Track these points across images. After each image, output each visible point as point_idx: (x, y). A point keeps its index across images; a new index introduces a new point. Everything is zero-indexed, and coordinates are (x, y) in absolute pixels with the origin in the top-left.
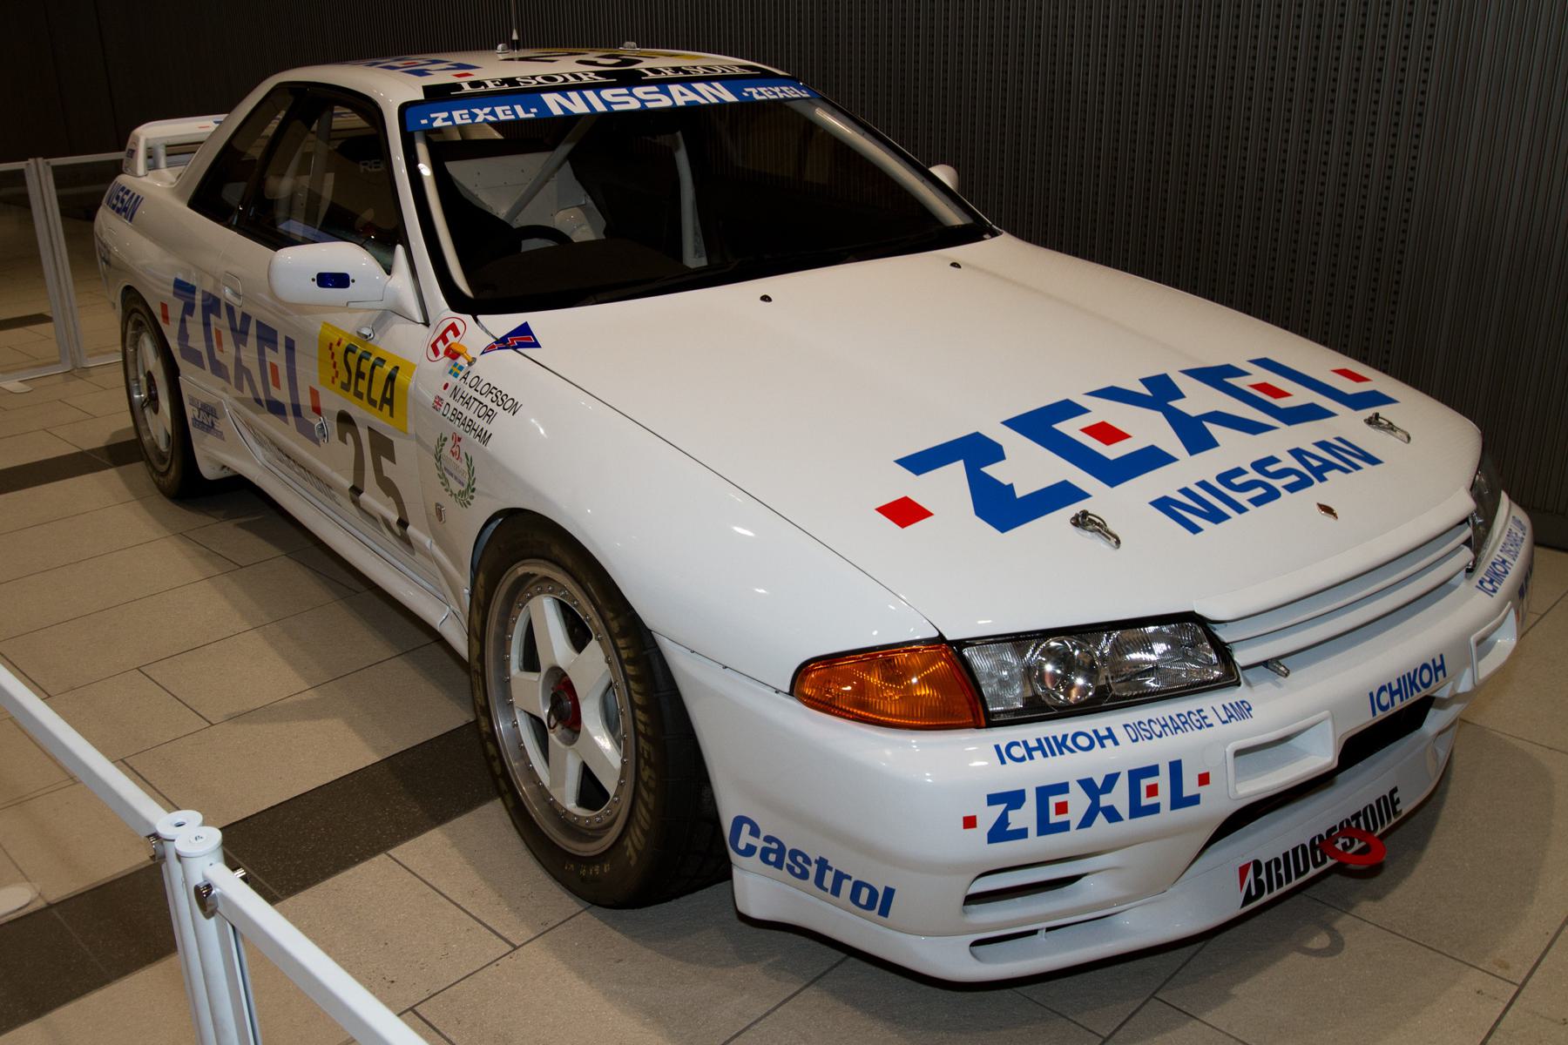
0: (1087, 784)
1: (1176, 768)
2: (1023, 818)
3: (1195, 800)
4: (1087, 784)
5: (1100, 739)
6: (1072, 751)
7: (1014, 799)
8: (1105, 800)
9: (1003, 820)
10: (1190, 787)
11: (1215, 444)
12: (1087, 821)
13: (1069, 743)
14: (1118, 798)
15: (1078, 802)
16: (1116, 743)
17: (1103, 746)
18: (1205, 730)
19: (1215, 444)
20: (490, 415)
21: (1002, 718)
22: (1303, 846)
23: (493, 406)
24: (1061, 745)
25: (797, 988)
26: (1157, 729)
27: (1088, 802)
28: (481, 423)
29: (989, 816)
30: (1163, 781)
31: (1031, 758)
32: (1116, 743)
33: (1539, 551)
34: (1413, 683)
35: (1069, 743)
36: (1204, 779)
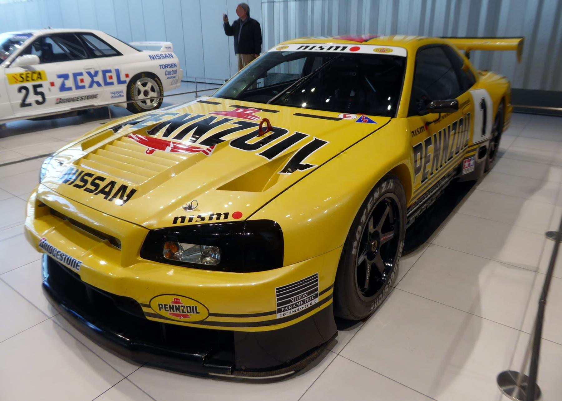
0: (89, 73)
1: (118, 72)
4: (89, 73)
8: (96, 79)
9: (63, 85)
12: (91, 86)
15: (87, 80)
30: (114, 75)
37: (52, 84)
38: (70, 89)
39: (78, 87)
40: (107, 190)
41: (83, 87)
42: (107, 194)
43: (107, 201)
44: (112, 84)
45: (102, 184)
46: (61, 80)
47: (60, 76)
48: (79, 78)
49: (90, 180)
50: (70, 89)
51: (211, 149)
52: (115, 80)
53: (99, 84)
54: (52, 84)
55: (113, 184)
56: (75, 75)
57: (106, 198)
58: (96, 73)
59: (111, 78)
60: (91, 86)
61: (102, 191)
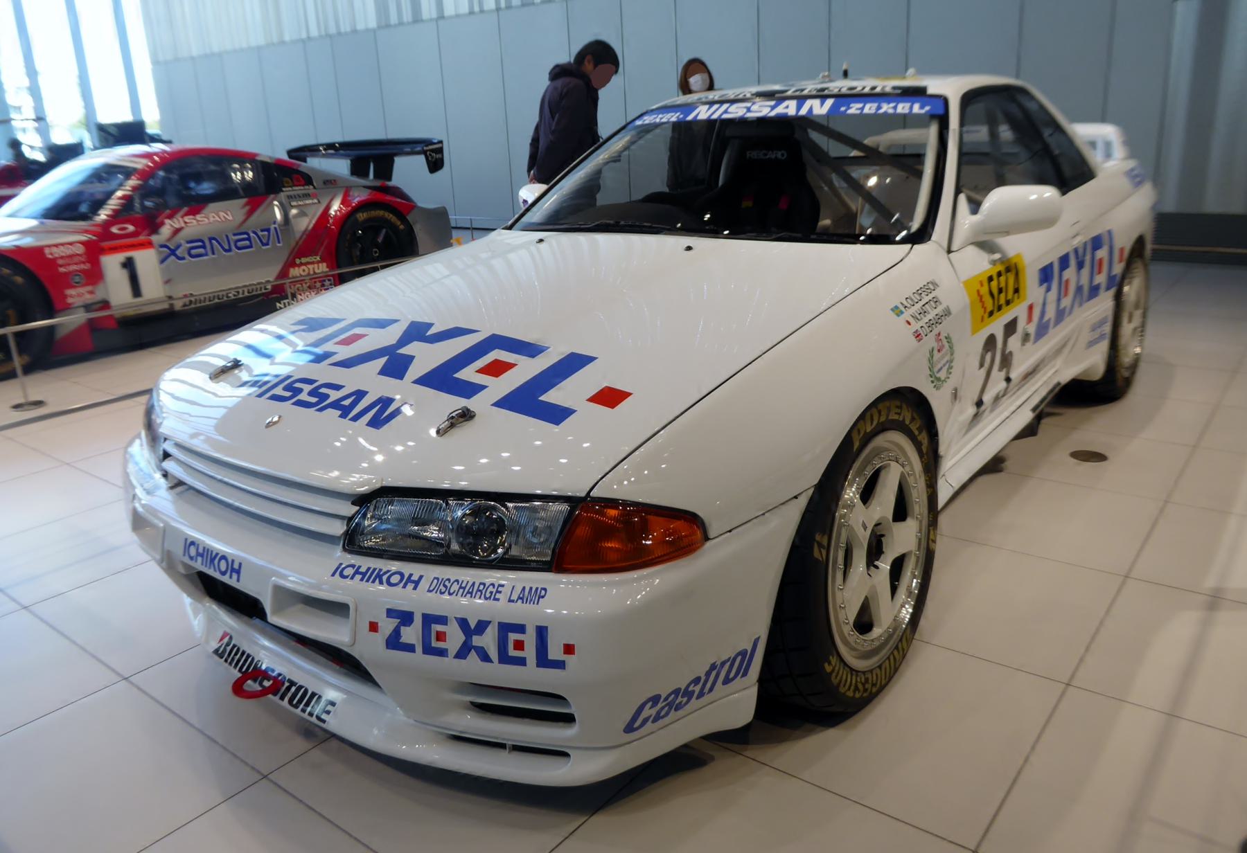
0: (463, 623)
1: (542, 632)
2: (411, 634)
3: (560, 665)
4: (463, 623)
5: (408, 581)
6: (381, 583)
7: (405, 618)
8: (477, 641)
9: (396, 633)
10: (555, 653)
11: (412, 358)
12: (462, 654)
13: (385, 578)
14: (488, 640)
15: (455, 639)
16: (415, 588)
17: (404, 587)
18: (491, 602)
19: (412, 358)
20: (936, 301)
21: (533, 565)
22: (306, 691)
23: (930, 296)
24: (379, 577)
25: (194, 721)
26: (455, 587)
27: (463, 638)
28: (939, 310)
29: (387, 626)
30: (530, 639)
31: (352, 578)
32: (415, 588)
33: (711, 535)
34: (212, 560)
35: (385, 578)
36: (569, 649)
37: (374, 627)
38: (410, 648)
39: (504, 658)
40: (347, 402)
41: (442, 653)
42: (345, 412)
43: (346, 421)
44: (522, 662)
45: (334, 395)
46: (393, 623)
47: (391, 613)
48: (513, 637)
49: (307, 388)
50: (410, 648)
51: (1100, 146)
52: (530, 652)
53: (485, 657)
54: (374, 627)
55: (360, 394)
56: (429, 620)
57: (343, 416)
58: (482, 626)
59: (519, 645)
60: (462, 654)
61: (336, 405)
